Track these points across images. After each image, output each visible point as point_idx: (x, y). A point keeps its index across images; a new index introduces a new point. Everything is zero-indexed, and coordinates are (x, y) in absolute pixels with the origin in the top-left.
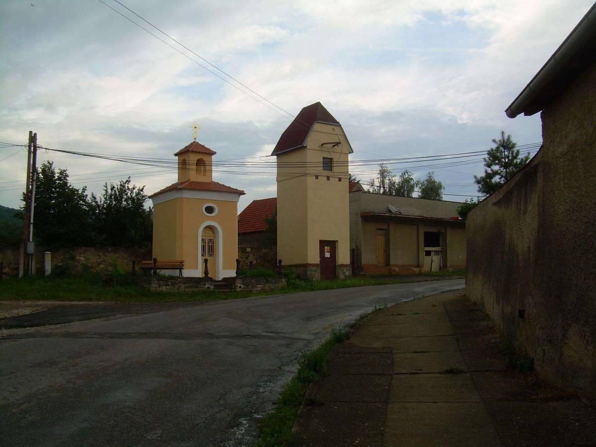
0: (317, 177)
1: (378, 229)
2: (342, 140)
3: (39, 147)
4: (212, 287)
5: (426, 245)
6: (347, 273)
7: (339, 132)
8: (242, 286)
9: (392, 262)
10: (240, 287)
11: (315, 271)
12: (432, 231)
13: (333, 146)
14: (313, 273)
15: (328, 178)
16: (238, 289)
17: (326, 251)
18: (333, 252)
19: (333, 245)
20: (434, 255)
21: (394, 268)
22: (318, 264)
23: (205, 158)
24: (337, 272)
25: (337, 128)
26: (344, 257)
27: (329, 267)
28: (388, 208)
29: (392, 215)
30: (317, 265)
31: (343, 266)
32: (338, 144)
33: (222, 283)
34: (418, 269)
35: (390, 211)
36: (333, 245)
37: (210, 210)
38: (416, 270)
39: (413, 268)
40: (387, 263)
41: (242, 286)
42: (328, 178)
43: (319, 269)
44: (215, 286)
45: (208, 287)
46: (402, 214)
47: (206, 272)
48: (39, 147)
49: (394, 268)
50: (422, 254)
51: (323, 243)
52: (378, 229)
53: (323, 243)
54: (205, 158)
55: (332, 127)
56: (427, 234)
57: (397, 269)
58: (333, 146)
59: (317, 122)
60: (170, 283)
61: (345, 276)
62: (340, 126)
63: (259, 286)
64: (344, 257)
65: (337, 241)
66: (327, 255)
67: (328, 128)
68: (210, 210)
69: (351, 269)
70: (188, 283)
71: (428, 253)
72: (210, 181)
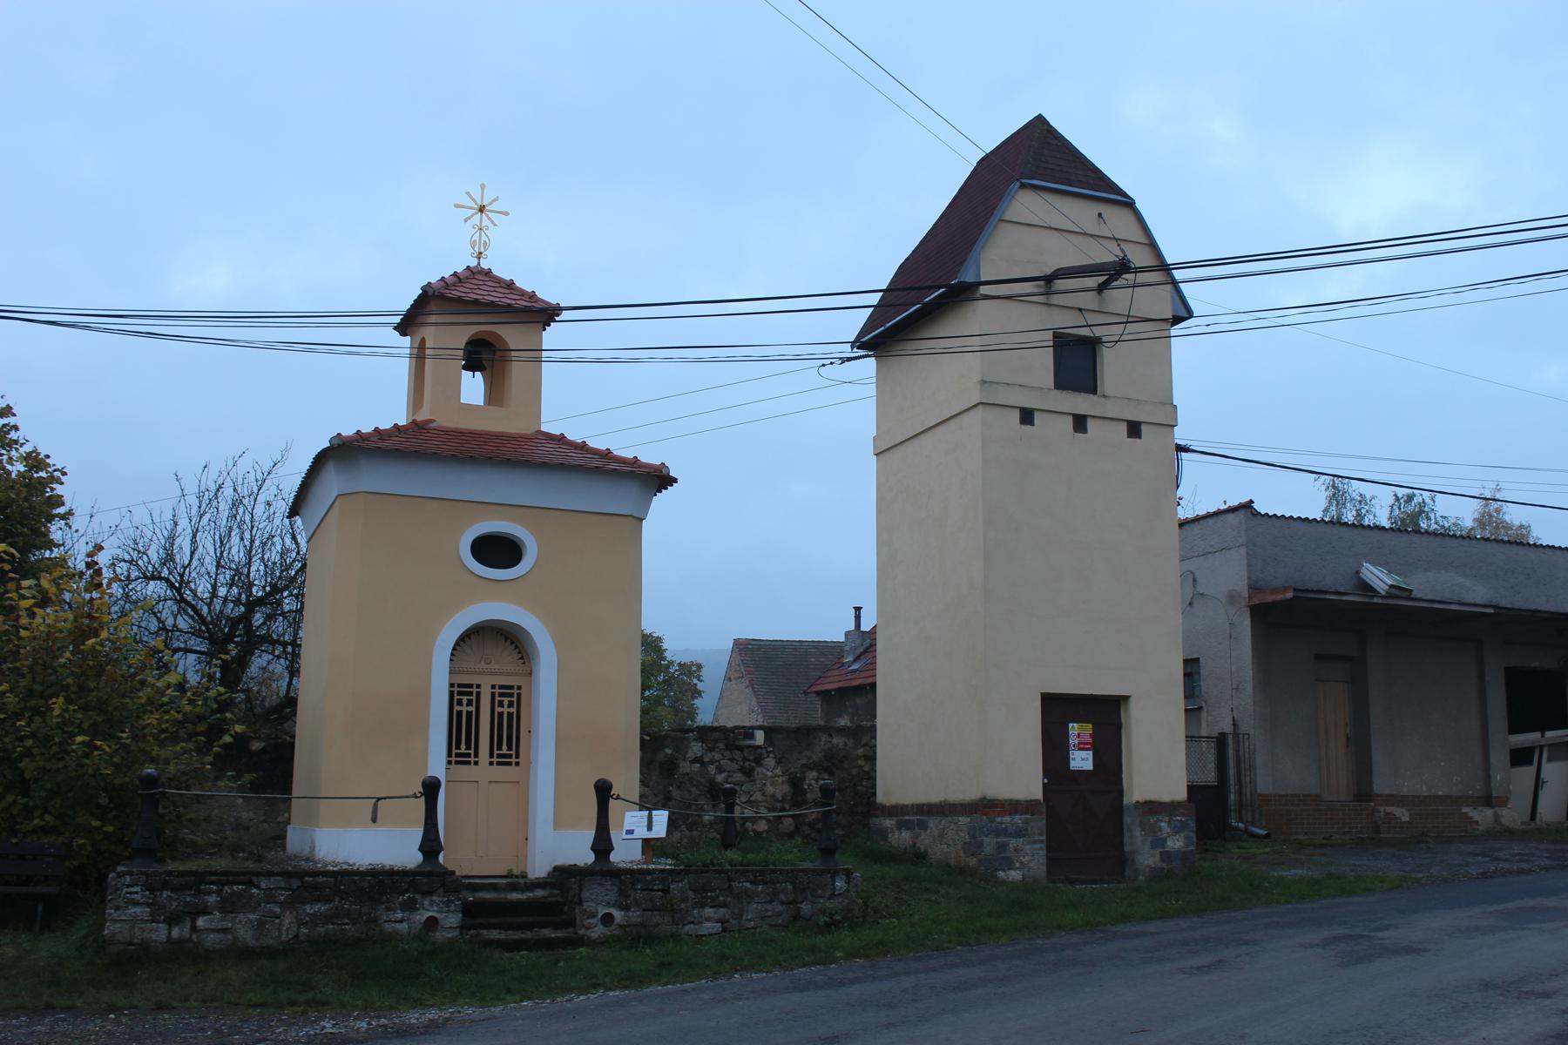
0: (1027, 416)
1: (1318, 657)
2: (1139, 257)
3: (1533, 816)
4: (452, 919)
5: (1513, 730)
6: (1176, 843)
7: (1130, 231)
8: (617, 914)
9: (1381, 786)
10: (607, 919)
11: (1018, 833)
12: (1536, 664)
13: (1101, 288)
14: (1013, 842)
15: (1080, 423)
16: (598, 931)
17: (1073, 741)
18: (1109, 745)
19: (1105, 714)
20: (1550, 760)
21: (1390, 809)
22: (1037, 802)
23: (512, 336)
24: (1126, 839)
25: (1118, 221)
26: (1158, 766)
27: (1082, 808)
28: (1358, 572)
29: (1375, 600)
30: (1028, 807)
31: (1151, 808)
32: (1123, 267)
33: (539, 893)
34: (1489, 812)
35: (1366, 588)
36: (1105, 714)
37: (497, 551)
38: (1483, 817)
39: (1465, 810)
40: (1363, 794)
41: (617, 914)
42: (1080, 423)
43: (1039, 824)
44: (469, 910)
45: (432, 923)
46: (1415, 594)
47: (430, 846)
48: (1533, 816)
49: (1390, 809)
50: (1499, 758)
51: (1059, 710)
52: (1318, 657)
53: (1059, 710)
54: (512, 336)
55: (1091, 210)
56: (1514, 678)
57: (1403, 814)
58: (1101, 288)
59: (1023, 186)
60: (212, 899)
61: (1166, 856)
62: (1129, 204)
63: (709, 911)
64: (1158, 766)
65: (1126, 698)
66: (1082, 760)
67: (1080, 213)
68: (497, 551)
69: (1193, 825)
70: (318, 900)
71: (1521, 757)
72: (530, 431)
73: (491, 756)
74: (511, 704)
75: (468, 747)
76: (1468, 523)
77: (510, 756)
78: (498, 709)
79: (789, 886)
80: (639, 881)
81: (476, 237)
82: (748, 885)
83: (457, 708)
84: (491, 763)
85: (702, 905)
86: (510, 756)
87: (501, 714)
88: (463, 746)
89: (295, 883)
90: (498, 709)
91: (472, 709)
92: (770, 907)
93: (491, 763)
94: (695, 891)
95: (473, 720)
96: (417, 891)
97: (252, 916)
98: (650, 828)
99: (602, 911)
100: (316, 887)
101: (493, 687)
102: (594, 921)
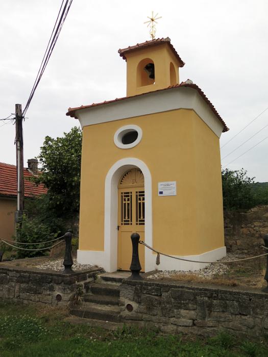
8: (135, 305)
10: (129, 307)
41: (135, 305)
63: (183, 312)
73: (137, 221)
74: (128, 200)
75: (128, 218)
76: (210, 278)
77: (129, 221)
78: (139, 202)
79: (236, 303)
80: (145, 289)
81: (152, 30)
82: (207, 299)
83: (124, 202)
84: (137, 224)
85: (179, 308)
86: (129, 221)
87: (125, 204)
88: (127, 217)
89: (18, 275)
90: (124, 202)
91: (129, 202)
92: (223, 315)
93: (137, 224)
94: (175, 299)
95: (130, 205)
96: (55, 283)
97: (6, 286)
98: (158, 263)
99: (127, 302)
100: (24, 277)
101: (137, 192)
102: (123, 307)
